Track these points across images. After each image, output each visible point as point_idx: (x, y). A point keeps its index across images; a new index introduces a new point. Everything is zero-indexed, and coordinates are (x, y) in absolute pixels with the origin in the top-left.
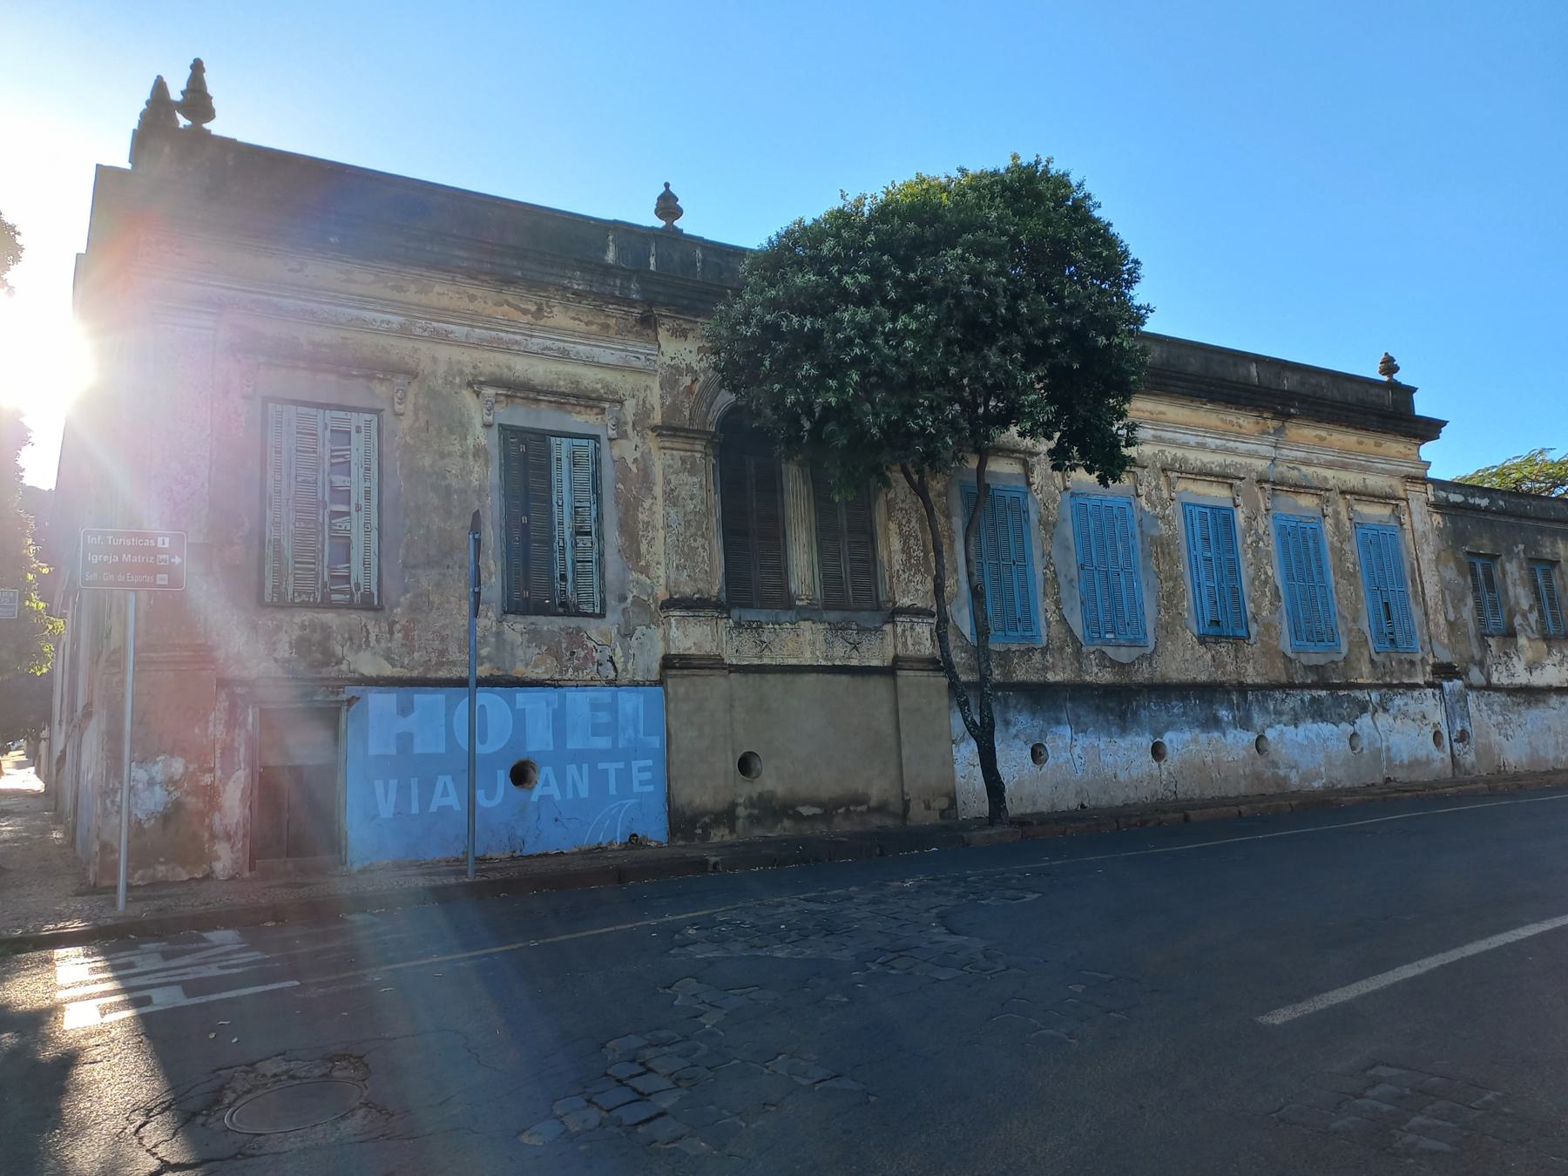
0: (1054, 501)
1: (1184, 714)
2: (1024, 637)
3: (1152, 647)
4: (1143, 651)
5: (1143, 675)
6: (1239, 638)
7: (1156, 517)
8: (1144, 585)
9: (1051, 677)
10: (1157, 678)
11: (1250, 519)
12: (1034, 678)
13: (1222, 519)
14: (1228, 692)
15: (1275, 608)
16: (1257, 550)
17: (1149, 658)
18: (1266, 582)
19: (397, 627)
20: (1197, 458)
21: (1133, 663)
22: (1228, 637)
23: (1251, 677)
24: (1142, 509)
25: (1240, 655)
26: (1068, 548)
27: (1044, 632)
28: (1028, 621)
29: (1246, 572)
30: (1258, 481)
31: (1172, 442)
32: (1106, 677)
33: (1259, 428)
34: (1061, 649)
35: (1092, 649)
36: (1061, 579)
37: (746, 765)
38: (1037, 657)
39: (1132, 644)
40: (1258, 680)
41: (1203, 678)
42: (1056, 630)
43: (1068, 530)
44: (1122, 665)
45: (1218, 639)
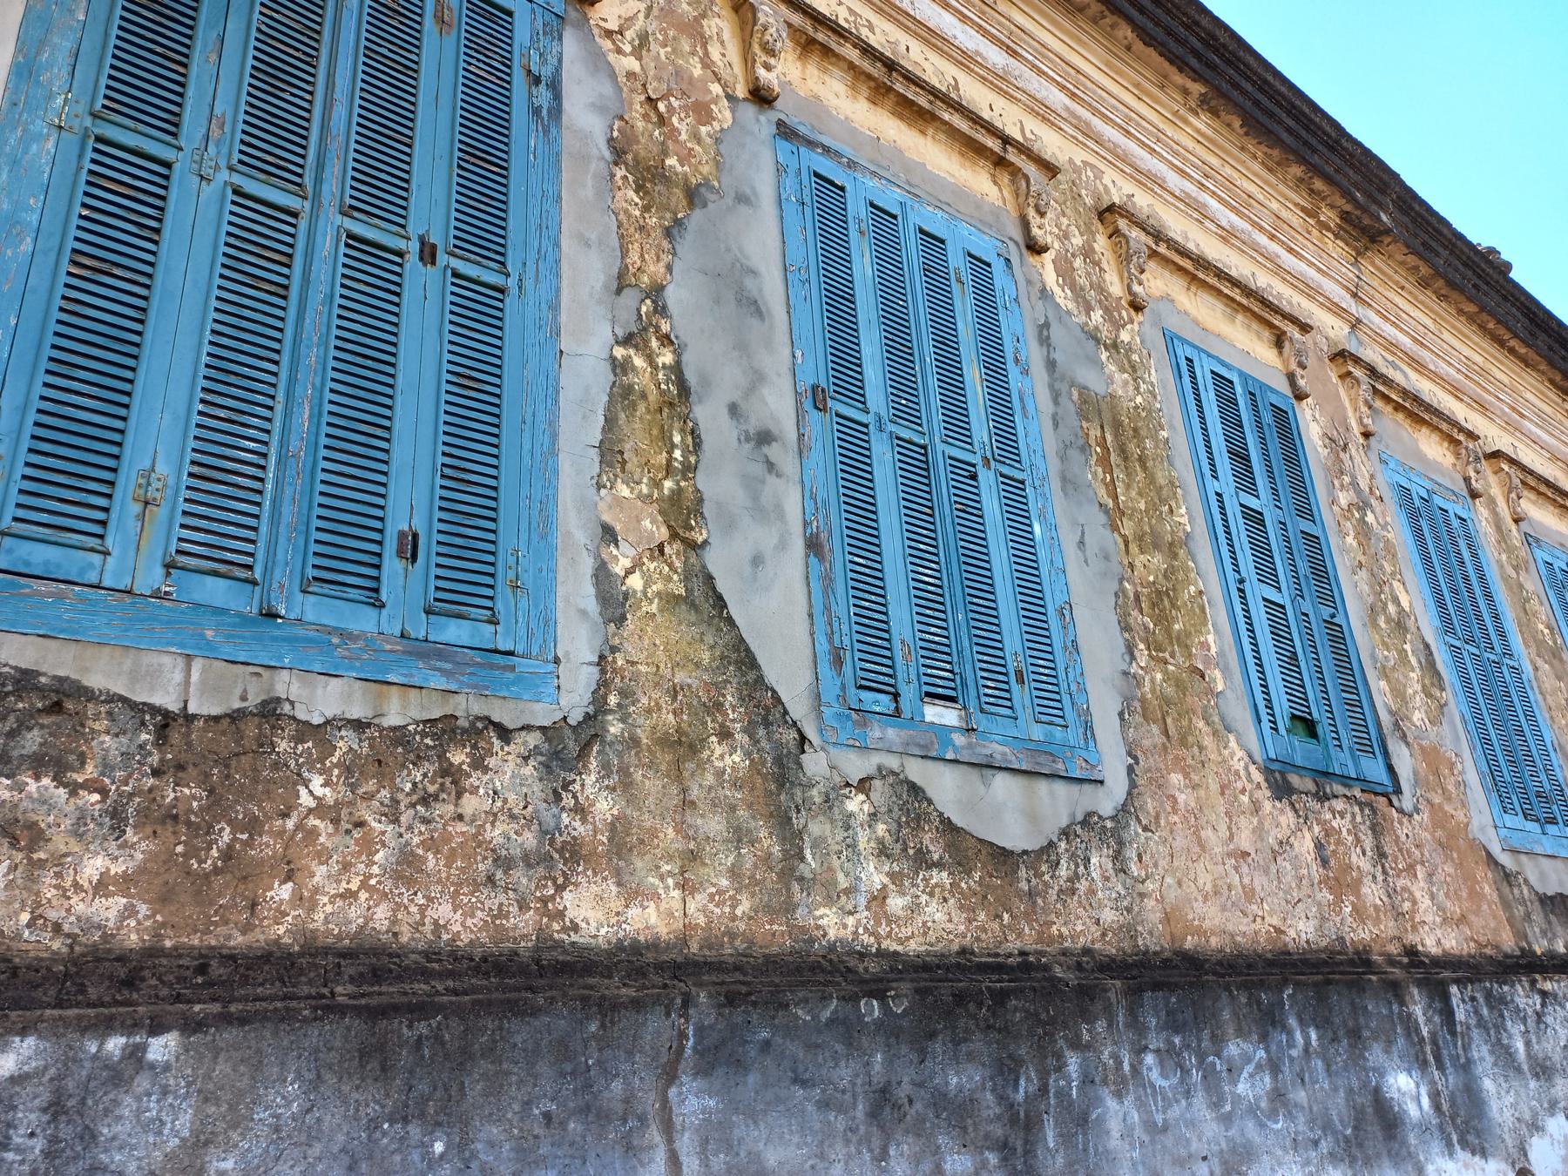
0: (703, 112)
1: (1278, 1096)
9: (593, 913)
10: (1153, 936)
12: (458, 920)
14: (1395, 990)
15: (1438, 712)
16: (1364, 531)
19: (118, 997)
23: (1437, 940)
24: (1044, 294)
26: (755, 307)
27: (577, 643)
28: (472, 555)
29: (1353, 589)
30: (1333, 359)
31: (1120, 158)
32: (931, 918)
33: (752, 431)
34: (683, 748)
35: (857, 766)
36: (709, 414)
38: (510, 774)
41: (1303, 930)
42: (657, 644)
44: (1003, 858)
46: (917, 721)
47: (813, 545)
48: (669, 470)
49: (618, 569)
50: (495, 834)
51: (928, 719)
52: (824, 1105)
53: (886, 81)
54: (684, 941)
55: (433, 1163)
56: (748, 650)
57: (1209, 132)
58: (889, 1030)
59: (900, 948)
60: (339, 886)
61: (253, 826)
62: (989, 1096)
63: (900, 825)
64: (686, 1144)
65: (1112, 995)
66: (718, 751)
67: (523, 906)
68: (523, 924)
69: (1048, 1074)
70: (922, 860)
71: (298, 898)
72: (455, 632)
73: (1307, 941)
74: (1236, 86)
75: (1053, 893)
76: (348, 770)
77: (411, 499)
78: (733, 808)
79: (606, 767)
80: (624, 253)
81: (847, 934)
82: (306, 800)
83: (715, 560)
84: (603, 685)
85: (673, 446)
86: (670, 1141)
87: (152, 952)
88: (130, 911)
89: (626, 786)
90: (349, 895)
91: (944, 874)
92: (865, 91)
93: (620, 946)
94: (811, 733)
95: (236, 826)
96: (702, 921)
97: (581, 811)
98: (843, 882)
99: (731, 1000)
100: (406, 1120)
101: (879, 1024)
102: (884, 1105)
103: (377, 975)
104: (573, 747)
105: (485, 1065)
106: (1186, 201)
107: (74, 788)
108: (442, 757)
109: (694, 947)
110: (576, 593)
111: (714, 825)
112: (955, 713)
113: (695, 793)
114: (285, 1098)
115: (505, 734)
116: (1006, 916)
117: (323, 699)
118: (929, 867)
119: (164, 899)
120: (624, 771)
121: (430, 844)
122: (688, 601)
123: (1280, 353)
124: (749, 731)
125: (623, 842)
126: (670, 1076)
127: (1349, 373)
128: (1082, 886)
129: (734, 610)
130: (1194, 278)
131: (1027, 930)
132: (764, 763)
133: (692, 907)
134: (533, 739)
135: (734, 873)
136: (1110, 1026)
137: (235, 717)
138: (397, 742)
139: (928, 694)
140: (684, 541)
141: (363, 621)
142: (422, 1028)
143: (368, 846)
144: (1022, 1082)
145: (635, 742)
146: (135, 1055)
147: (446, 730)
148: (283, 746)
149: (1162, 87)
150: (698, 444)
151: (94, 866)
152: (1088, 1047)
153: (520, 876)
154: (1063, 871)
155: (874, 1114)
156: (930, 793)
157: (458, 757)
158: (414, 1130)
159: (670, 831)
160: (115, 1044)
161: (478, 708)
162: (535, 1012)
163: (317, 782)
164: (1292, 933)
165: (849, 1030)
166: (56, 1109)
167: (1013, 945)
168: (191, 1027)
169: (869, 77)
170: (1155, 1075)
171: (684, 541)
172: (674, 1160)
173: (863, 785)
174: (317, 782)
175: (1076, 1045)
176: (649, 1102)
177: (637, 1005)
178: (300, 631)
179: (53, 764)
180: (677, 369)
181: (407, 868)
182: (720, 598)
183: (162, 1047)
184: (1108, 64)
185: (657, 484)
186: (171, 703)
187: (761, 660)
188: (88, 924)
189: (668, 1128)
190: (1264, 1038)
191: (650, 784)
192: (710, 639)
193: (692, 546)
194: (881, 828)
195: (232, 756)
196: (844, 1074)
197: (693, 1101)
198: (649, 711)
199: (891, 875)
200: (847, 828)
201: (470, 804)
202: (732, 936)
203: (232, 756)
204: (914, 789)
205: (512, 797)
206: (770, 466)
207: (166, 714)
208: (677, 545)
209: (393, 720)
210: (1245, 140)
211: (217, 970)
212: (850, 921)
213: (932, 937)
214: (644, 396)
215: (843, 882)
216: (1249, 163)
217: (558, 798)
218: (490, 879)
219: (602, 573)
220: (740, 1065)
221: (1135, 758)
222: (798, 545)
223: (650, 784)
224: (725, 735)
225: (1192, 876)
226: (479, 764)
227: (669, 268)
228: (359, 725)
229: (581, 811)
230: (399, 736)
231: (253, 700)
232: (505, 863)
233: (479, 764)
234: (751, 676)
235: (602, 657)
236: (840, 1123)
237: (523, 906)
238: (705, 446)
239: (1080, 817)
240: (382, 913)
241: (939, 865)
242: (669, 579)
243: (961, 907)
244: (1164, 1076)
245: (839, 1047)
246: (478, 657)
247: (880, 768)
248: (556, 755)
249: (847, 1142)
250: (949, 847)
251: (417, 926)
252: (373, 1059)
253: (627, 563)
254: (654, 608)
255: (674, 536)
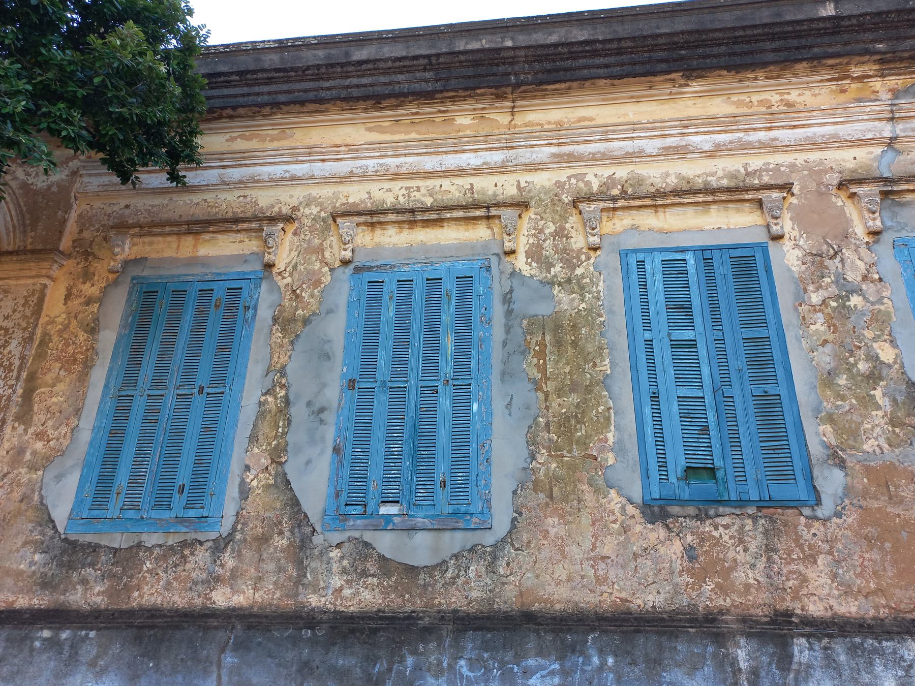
0: (317, 283)
2: (181, 520)
3: (501, 524)
4: (472, 538)
5: (470, 590)
6: (786, 505)
7: (551, 283)
8: (498, 405)
9: (221, 598)
10: (508, 598)
11: (817, 261)
12: (179, 600)
13: (746, 267)
17: (493, 555)
18: (873, 378)
20: (657, 174)
21: (442, 566)
22: (742, 503)
23: (822, 593)
25: (782, 545)
26: (327, 356)
27: (230, 510)
28: (200, 488)
29: (806, 356)
32: (366, 597)
34: (264, 540)
36: (298, 411)
37: (528, 408)
38: (202, 556)
39: (445, 524)
40: (850, 608)
41: (652, 599)
42: (264, 503)
43: (336, 329)
44: (412, 570)
45: (706, 508)
46: (375, 514)
47: (336, 450)
48: (276, 437)
49: (248, 480)
50: (194, 575)
51: (381, 513)
52: (279, 665)
53: (412, 216)
54: (252, 607)
55: (149, 669)
56: (297, 499)
57: (705, 88)
58: (313, 642)
59: (345, 610)
60: (154, 591)
61: (132, 577)
62: (358, 669)
63: (355, 560)
64: (224, 672)
65: (444, 633)
66: (277, 539)
67: (199, 596)
68: (198, 602)
69: (394, 664)
70: (365, 574)
71: (140, 596)
72: (192, 513)
73: (654, 607)
74: (705, 57)
75: (439, 585)
76: (156, 559)
77: (184, 476)
78: (279, 560)
79: (233, 550)
80: (271, 358)
81: (321, 604)
82: (145, 569)
83: (288, 468)
84: (237, 522)
85: (279, 427)
86: (219, 670)
87: (106, 610)
88: (103, 600)
89: (239, 556)
90: (153, 594)
91: (375, 579)
92: (406, 226)
93: (229, 609)
94: (318, 528)
95: (128, 577)
96: (260, 600)
97: (222, 566)
98: (322, 584)
99: (249, 627)
100: (144, 657)
101: (309, 639)
102: (305, 668)
103: (152, 616)
104: (223, 545)
105: (167, 643)
106: (668, 153)
107: (96, 570)
108: (182, 553)
109: (255, 609)
110: (232, 491)
111: (271, 566)
112: (398, 508)
113: (265, 556)
114: (116, 648)
115: (201, 543)
116: (407, 596)
117: (152, 539)
118: (367, 576)
119: (110, 597)
120: (239, 551)
121: (175, 579)
122: (275, 485)
123: (763, 212)
124: (292, 531)
125: (235, 574)
126: (223, 651)
127: (854, 194)
128: (460, 581)
129: (293, 485)
130: (655, 207)
131: (419, 602)
132: (295, 542)
133: (257, 596)
134: (210, 544)
135: (275, 583)
136: (439, 646)
137: (131, 548)
138: (170, 549)
139: (383, 502)
140: (277, 463)
141: (167, 515)
142: (152, 632)
143: (158, 581)
144: (378, 666)
145: (245, 540)
146: (87, 635)
147: (184, 544)
148: (141, 554)
149: (650, 88)
150: (289, 424)
151: (97, 589)
152: (422, 654)
153: (200, 588)
154: (449, 574)
155: (299, 671)
156: (374, 545)
157: (187, 552)
158: (146, 660)
159: (253, 570)
160: (84, 632)
161: (194, 536)
162: (184, 629)
163: (148, 563)
164: (639, 602)
165: (295, 641)
166: (72, 646)
167: (409, 608)
168: (98, 629)
169: (404, 222)
170: (465, 671)
171: (277, 463)
172: (219, 677)
173: (339, 546)
174: (148, 563)
175: (414, 652)
176: (215, 658)
177: (216, 628)
178: (150, 521)
179: (92, 565)
180: (287, 395)
181: (168, 586)
182: (288, 481)
183: (92, 634)
184: (603, 100)
185: (270, 444)
186: (116, 546)
187: (301, 503)
188: (95, 603)
189: (219, 667)
190: (561, 658)
191: (247, 554)
192: (281, 498)
193: (281, 464)
194: (345, 562)
195: (127, 559)
196: (290, 656)
197: (229, 659)
198: (252, 529)
199: (347, 581)
200: (328, 563)
201: (188, 566)
202: (271, 605)
203: (127, 559)
204: (367, 545)
205: (201, 563)
206: (322, 421)
207: (116, 549)
208: (274, 465)
209: (170, 543)
210: (740, 75)
211: (116, 615)
212: (323, 599)
213: (363, 605)
214: (270, 411)
215: (322, 584)
216: (754, 84)
217: (215, 561)
218: (191, 589)
219: (243, 483)
220: (248, 649)
221: (520, 514)
222: (330, 451)
223: (247, 554)
224: (281, 533)
225: (550, 572)
226: (192, 554)
227: (290, 357)
228: (161, 546)
229: (222, 566)
230: (171, 548)
231: (136, 542)
232: (195, 583)
233: (192, 554)
234: (297, 508)
235: (238, 513)
236: (285, 672)
237: (199, 596)
238: (293, 423)
239: (468, 547)
240: (160, 599)
241: (373, 576)
242: (268, 479)
243: (382, 593)
244: (470, 670)
245: (289, 646)
246: (796, 412)
247: (349, 538)
248: (216, 548)
249: (286, 679)
250: (380, 568)
251: (168, 603)
252: (138, 640)
253: (252, 477)
254: (260, 491)
255: (273, 461)
